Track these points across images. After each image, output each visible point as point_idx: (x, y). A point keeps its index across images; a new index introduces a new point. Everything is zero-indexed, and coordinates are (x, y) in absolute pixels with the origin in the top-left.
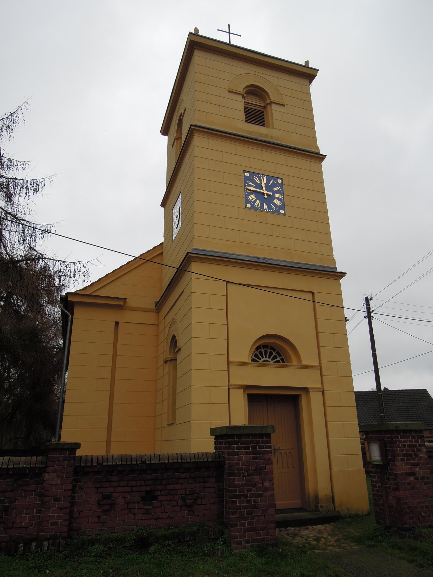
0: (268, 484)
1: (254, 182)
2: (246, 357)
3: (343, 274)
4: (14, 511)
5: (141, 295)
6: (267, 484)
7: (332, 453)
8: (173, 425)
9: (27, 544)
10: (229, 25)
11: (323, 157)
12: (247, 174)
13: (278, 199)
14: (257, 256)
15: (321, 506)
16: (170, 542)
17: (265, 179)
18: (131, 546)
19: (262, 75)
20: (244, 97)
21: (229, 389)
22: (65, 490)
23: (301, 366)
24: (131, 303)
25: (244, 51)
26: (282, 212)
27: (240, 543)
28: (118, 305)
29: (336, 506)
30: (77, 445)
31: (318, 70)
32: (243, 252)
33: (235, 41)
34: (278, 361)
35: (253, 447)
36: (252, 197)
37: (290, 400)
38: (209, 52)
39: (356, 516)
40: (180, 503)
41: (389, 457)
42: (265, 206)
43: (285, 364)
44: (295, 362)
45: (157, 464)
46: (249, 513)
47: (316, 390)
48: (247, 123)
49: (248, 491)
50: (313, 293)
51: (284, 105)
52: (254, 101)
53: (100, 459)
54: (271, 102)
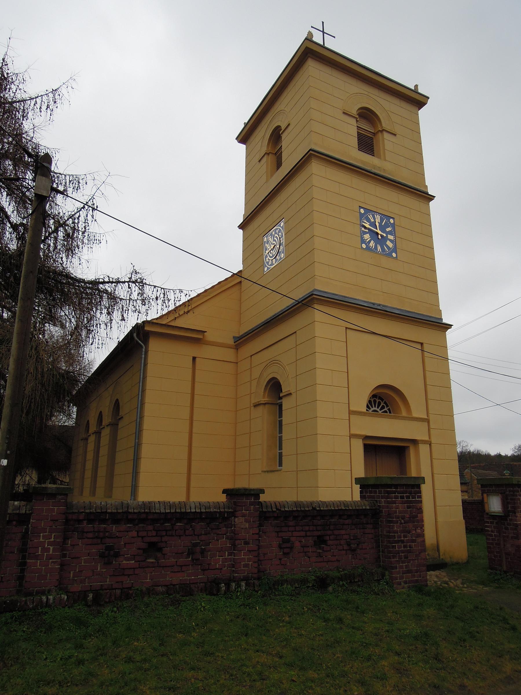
0: (419, 531)
1: (368, 220)
3: (449, 326)
4: (209, 553)
5: (220, 329)
6: (419, 531)
7: (438, 504)
8: (279, 472)
10: (323, 23)
11: (431, 198)
12: (362, 211)
13: (391, 241)
14: (373, 301)
15: (428, 554)
16: (345, 583)
17: (379, 217)
18: (313, 586)
19: (372, 96)
20: (357, 121)
22: (253, 534)
24: (210, 336)
25: (347, 60)
26: (394, 255)
27: (400, 584)
28: (195, 338)
29: (441, 554)
30: (262, 491)
31: (428, 98)
32: (360, 296)
33: (330, 44)
34: (386, 412)
35: (408, 497)
36: (367, 237)
37: (396, 451)
38: (316, 60)
39: (457, 563)
40: (346, 547)
41: (510, 509)
42: (379, 248)
43: (392, 414)
44: (404, 413)
45: (326, 510)
46: (406, 557)
47: (424, 442)
48: (360, 152)
49: (405, 536)
50: (422, 344)
51: (395, 135)
52: (366, 126)
53: (278, 505)
54: (383, 130)
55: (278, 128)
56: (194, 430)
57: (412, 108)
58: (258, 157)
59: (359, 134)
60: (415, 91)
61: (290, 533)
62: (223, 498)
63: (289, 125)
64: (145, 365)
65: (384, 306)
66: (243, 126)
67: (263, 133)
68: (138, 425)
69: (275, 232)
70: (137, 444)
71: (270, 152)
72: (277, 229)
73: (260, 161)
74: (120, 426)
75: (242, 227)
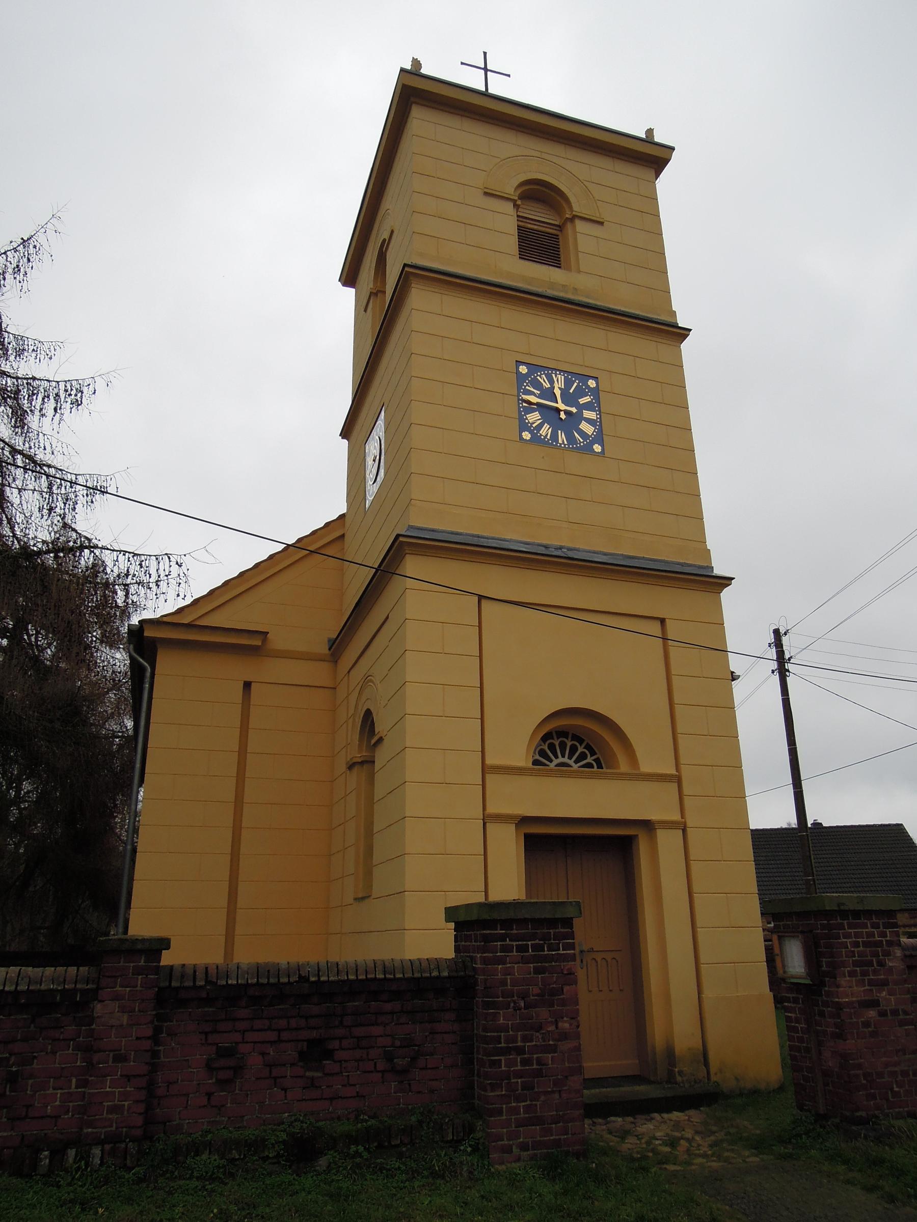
0: (567, 1025)
1: (537, 385)
2: (521, 757)
3: (726, 581)
4: (30, 1082)
5: (300, 624)
6: (565, 1025)
7: (703, 958)
8: (367, 901)
10: (485, 53)
11: (684, 333)
12: (523, 369)
13: (589, 421)
14: (545, 542)
15: (680, 1073)
16: (361, 1148)
17: (561, 378)
18: (278, 1156)
19: (555, 160)
20: (516, 206)
21: (484, 824)
22: (137, 1038)
23: (636, 774)
24: (278, 641)
25: (516, 107)
26: (597, 448)
27: (508, 1150)
28: (250, 645)
29: (712, 1071)
30: (164, 943)
31: (673, 149)
32: (514, 534)
33: (498, 87)
34: (589, 766)
35: (536, 948)
36: (534, 418)
37: (614, 848)
38: (442, 110)
39: (755, 1092)
40: (381, 1065)
41: (824, 968)
42: (562, 437)
43: (604, 770)
44: (624, 766)
45: (333, 982)
46: (527, 1087)
47: (669, 825)
48: (522, 261)
49: (525, 1039)
50: (662, 621)
51: (602, 223)
52: (538, 214)
53: (212, 972)
54: (575, 217)
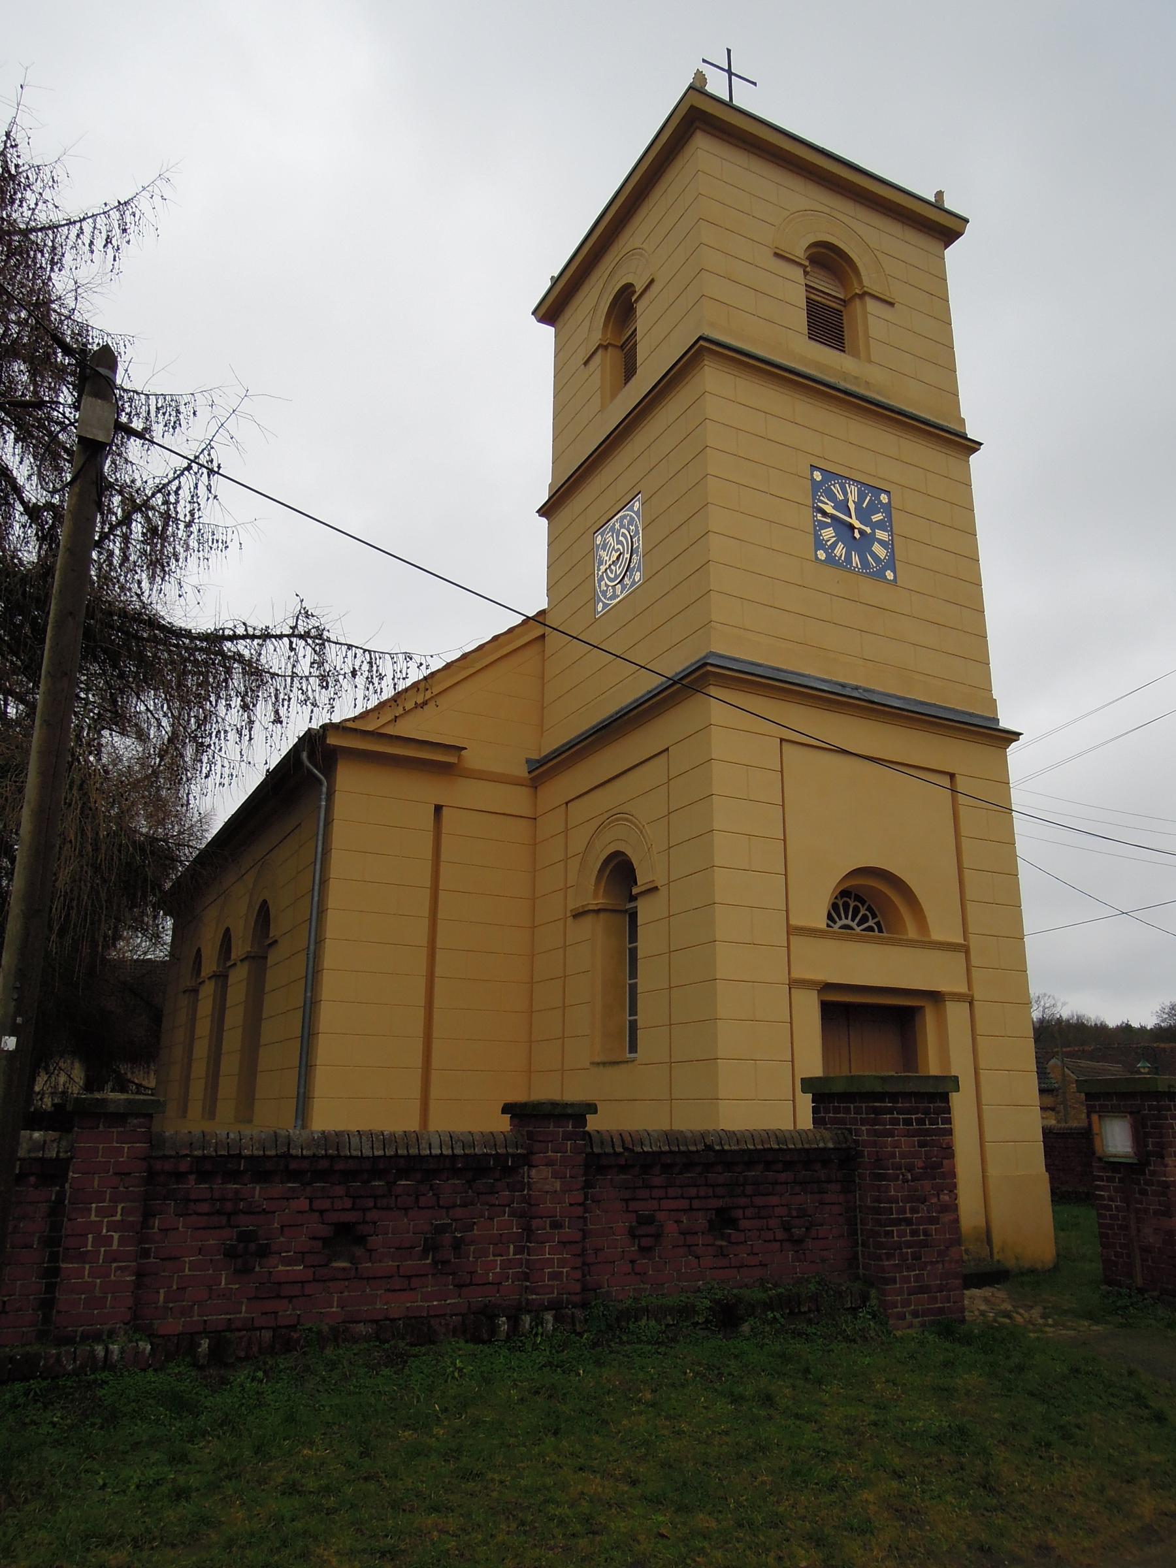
0: (947, 1198)
1: (832, 497)
3: (1014, 736)
4: (472, 1248)
5: (497, 742)
6: (945, 1198)
7: (988, 1137)
8: (630, 1065)
9: (514, 1321)
10: (729, 51)
11: (973, 446)
12: (818, 476)
13: (882, 543)
14: (841, 680)
15: (966, 1251)
16: (778, 1316)
17: (855, 489)
18: (707, 1321)
19: (839, 216)
20: (806, 273)
22: (571, 1205)
24: (473, 759)
25: (782, 136)
26: (890, 575)
27: (902, 1317)
28: (439, 762)
29: (996, 1250)
30: (592, 1108)
31: (967, 221)
32: (812, 668)
33: (744, 98)
34: (870, 929)
35: (921, 1122)
36: (828, 534)
37: (893, 1017)
38: (712, 135)
39: (1032, 1271)
40: (780, 1234)
41: (1150, 1148)
42: (856, 560)
43: (885, 935)
44: (912, 933)
45: (735, 1151)
46: (917, 1257)
47: (958, 997)
48: (813, 343)
49: (914, 1210)
50: (952, 776)
51: (892, 304)
52: (825, 284)
53: (628, 1139)
54: (866, 293)
55: (628, 288)
56: (439, 971)
57: (931, 244)
58: (583, 355)
59: (809, 301)
60: (938, 205)
61: (655, 1202)
62: (504, 1124)
63: (652, 281)
64: (328, 822)
65: (866, 690)
66: (549, 284)
67: (595, 300)
68: (311, 960)
69: (621, 522)
70: (308, 1003)
71: (609, 344)
72: (625, 517)
73: (586, 363)
74: (270, 961)
75: (546, 511)
